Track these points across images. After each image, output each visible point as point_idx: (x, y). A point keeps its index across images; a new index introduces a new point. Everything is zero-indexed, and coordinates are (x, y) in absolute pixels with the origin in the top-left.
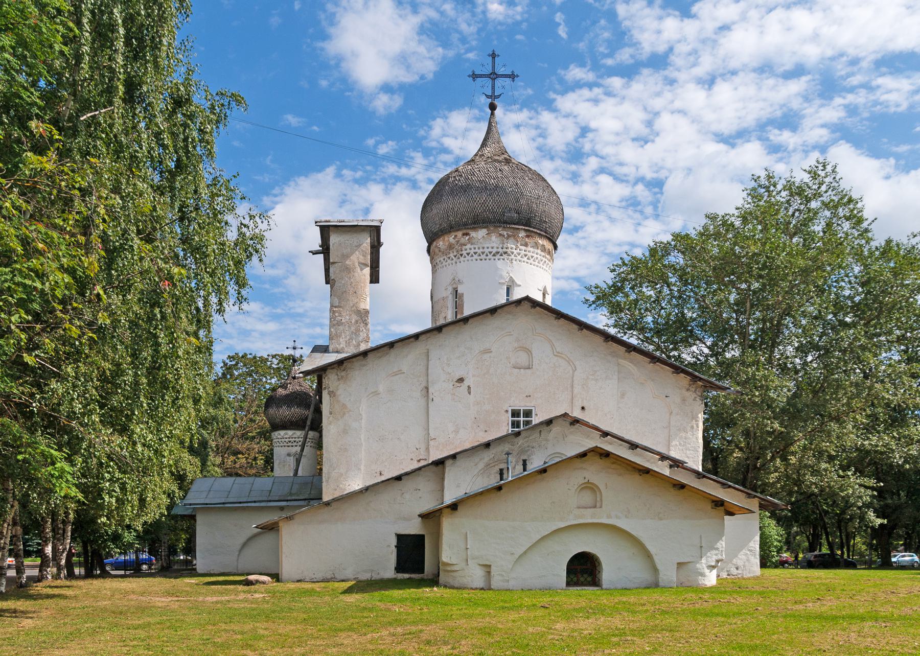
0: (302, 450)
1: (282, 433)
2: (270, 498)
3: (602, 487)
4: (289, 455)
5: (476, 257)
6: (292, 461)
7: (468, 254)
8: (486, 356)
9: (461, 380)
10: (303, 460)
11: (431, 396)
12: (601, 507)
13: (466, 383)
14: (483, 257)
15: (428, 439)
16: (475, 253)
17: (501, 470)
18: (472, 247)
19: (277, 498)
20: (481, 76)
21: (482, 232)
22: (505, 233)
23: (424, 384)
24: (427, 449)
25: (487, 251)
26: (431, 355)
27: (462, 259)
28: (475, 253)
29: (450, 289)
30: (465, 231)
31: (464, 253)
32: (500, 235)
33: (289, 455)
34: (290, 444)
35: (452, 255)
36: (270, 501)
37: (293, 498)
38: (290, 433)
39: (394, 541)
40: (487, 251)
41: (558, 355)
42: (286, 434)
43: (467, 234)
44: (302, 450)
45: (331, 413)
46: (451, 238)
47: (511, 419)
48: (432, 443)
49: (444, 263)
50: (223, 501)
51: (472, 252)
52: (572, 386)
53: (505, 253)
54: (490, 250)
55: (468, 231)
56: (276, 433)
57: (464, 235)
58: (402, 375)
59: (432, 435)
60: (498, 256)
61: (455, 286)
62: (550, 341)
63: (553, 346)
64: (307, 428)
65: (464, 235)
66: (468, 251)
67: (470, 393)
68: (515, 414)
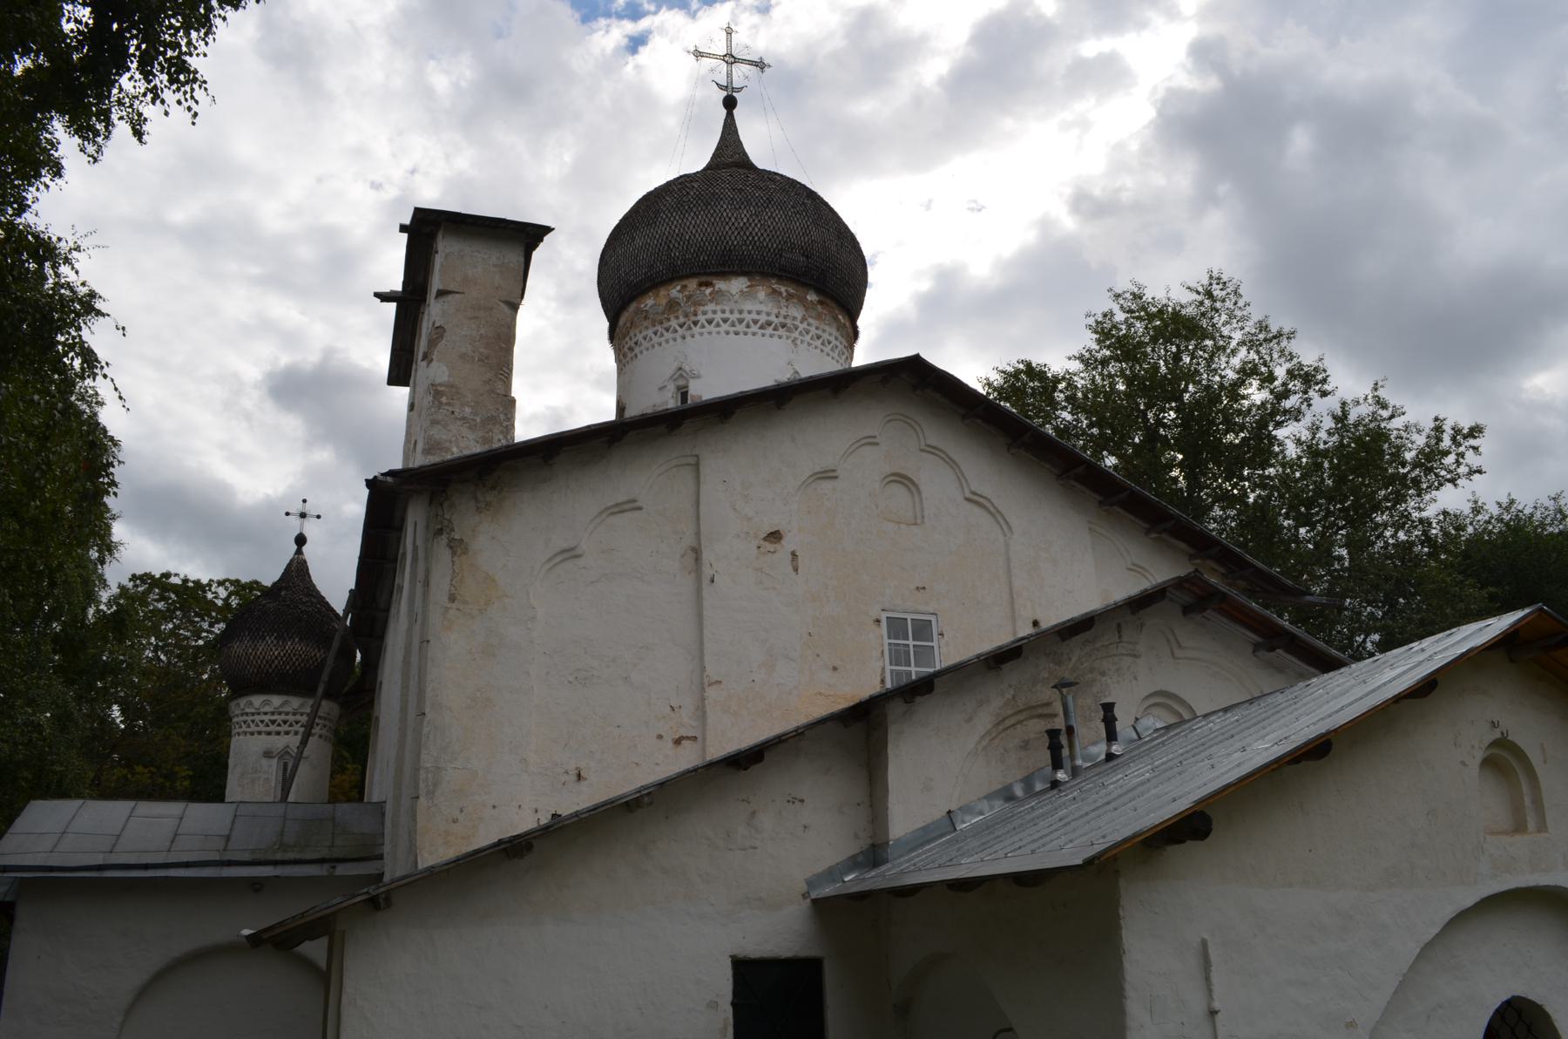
0: (304, 743)
1: (257, 700)
2: (228, 857)
3: (1534, 757)
4: (268, 754)
5: (725, 327)
6: (272, 768)
7: (710, 322)
8: (826, 486)
9: (775, 536)
10: (303, 769)
11: (707, 572)
12: (1542, 827)
13: (788, 544)
14: (741, 328)
15: (703, 684)
16: (725, 321)
17: (1053, 734)
18: (718, 308)
19: (247, 857)
20: (709, 55)
21: (737, 285)
22: (783, 289)
23: (689, 540)
24: (701, 712)
25: (748, 317)
26: (704, 470)
27: (696, 330)
28: (725, 321)
29: (672, 387)
30: (704, 279)
31: (702, 319)
32: (774, 291)
33: (268, 754)
34: (272, 728)
35: (674, 323)
36: (230, 863)
37: (291, 856)
38: (277, 700)
39: (723, 984)
40: (748, 317)
41: (975, 500)
42: (266, 703)
43: (708, 284)
44: (304, 743)
45: (452, 599)
46: (675, 291)
47: (887, 641)
48: (711, 693)
49: (656, 339)
50: (99, 860)
51: (718, 317)
52: (1009, 570)
53: (783, 326)
54: (754, 316)
55: (709, 279)
56: (243, 701)
57: (701, 285)
58: (636, 514)
59: (712, 671)
60: (769, 330)
61: (681, 382)
62: (952, 463)
63: (961, 478)
64: (320, 690)
65: (701, 285)
66: (710, 316)
67: (796, 570)
68: (896, 627)
